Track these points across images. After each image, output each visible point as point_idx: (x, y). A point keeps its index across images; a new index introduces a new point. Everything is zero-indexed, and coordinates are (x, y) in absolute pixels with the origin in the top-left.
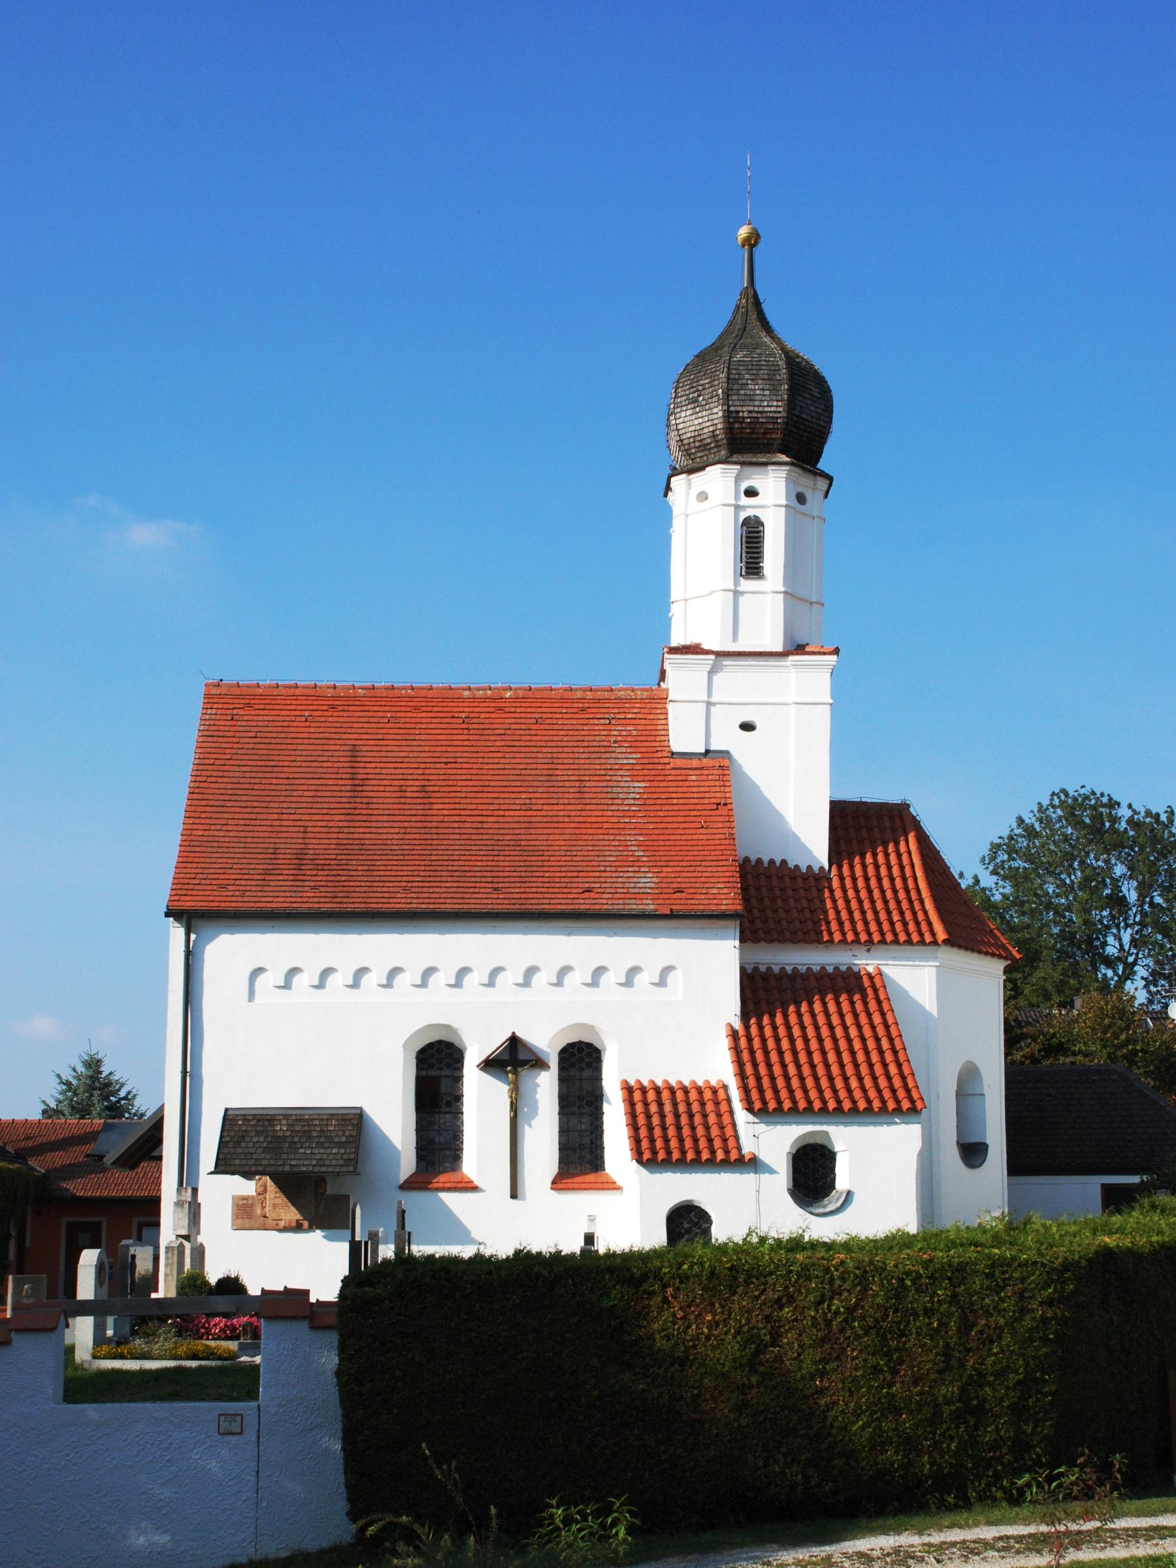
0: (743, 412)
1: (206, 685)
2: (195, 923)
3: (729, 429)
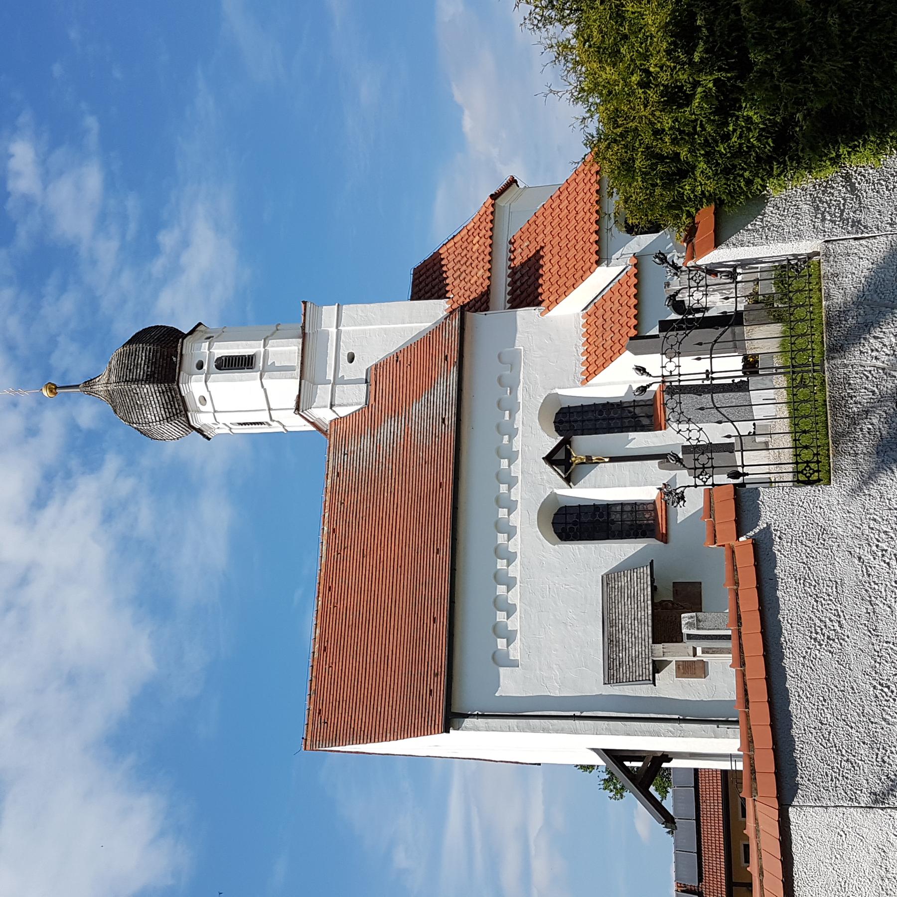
0: (147, 372)
3: (159, 381)
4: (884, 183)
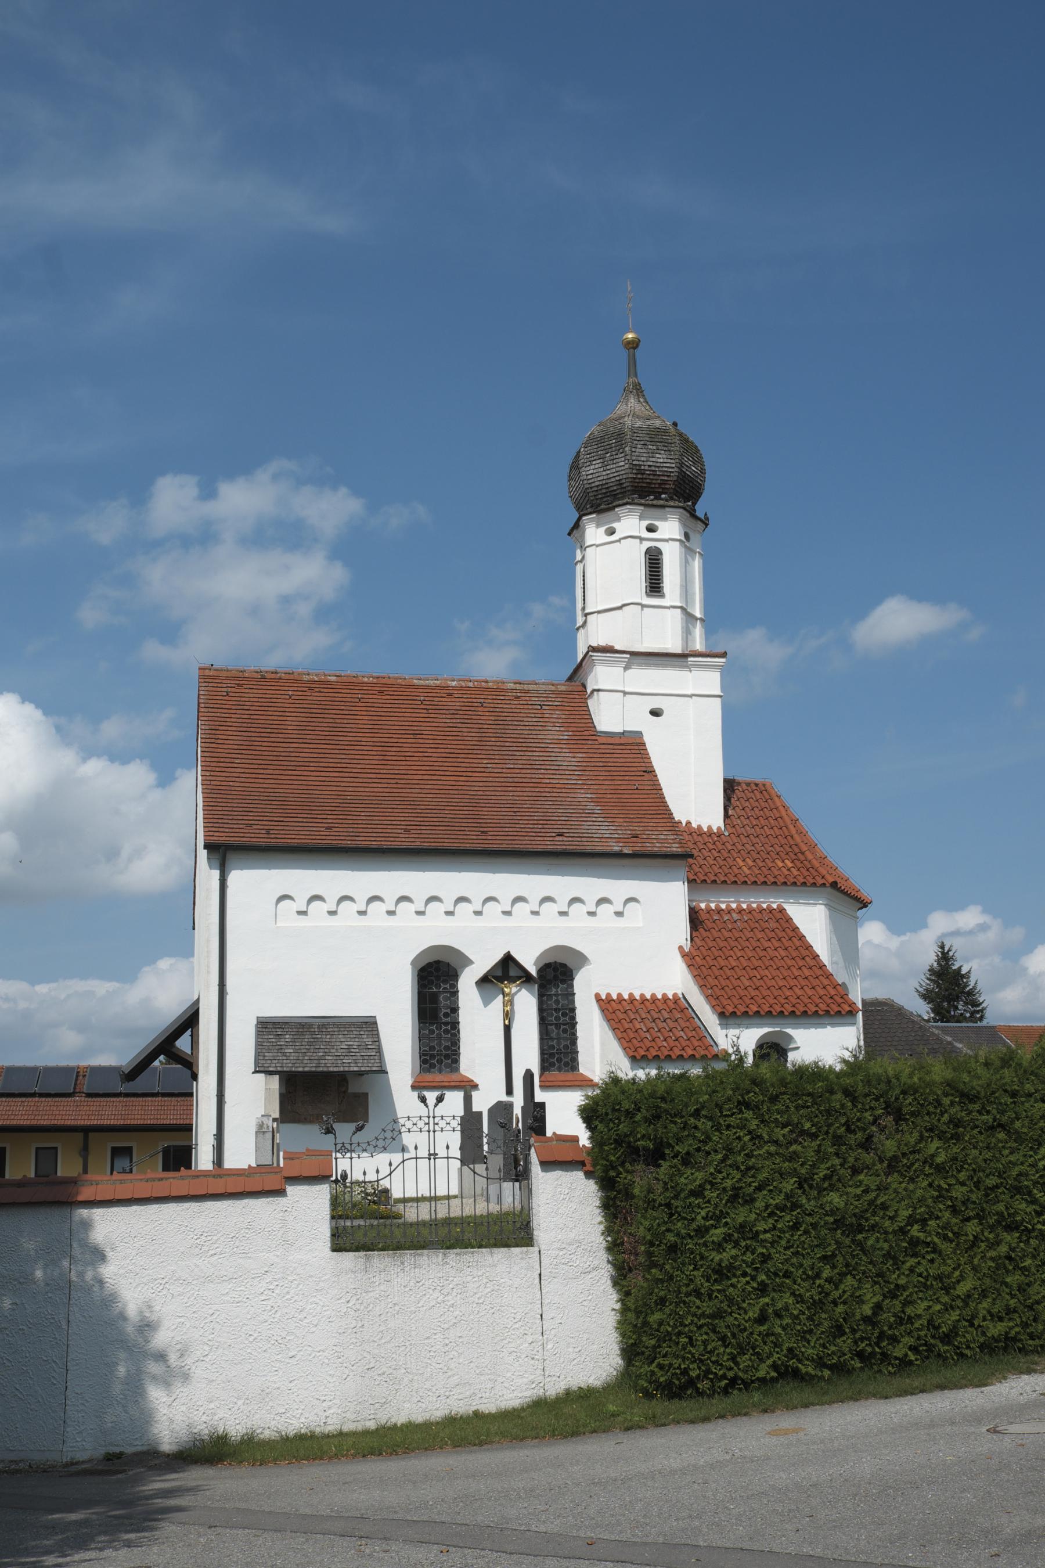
1: (200, 669)
2: (232, 858)
4: (590, 1298)
